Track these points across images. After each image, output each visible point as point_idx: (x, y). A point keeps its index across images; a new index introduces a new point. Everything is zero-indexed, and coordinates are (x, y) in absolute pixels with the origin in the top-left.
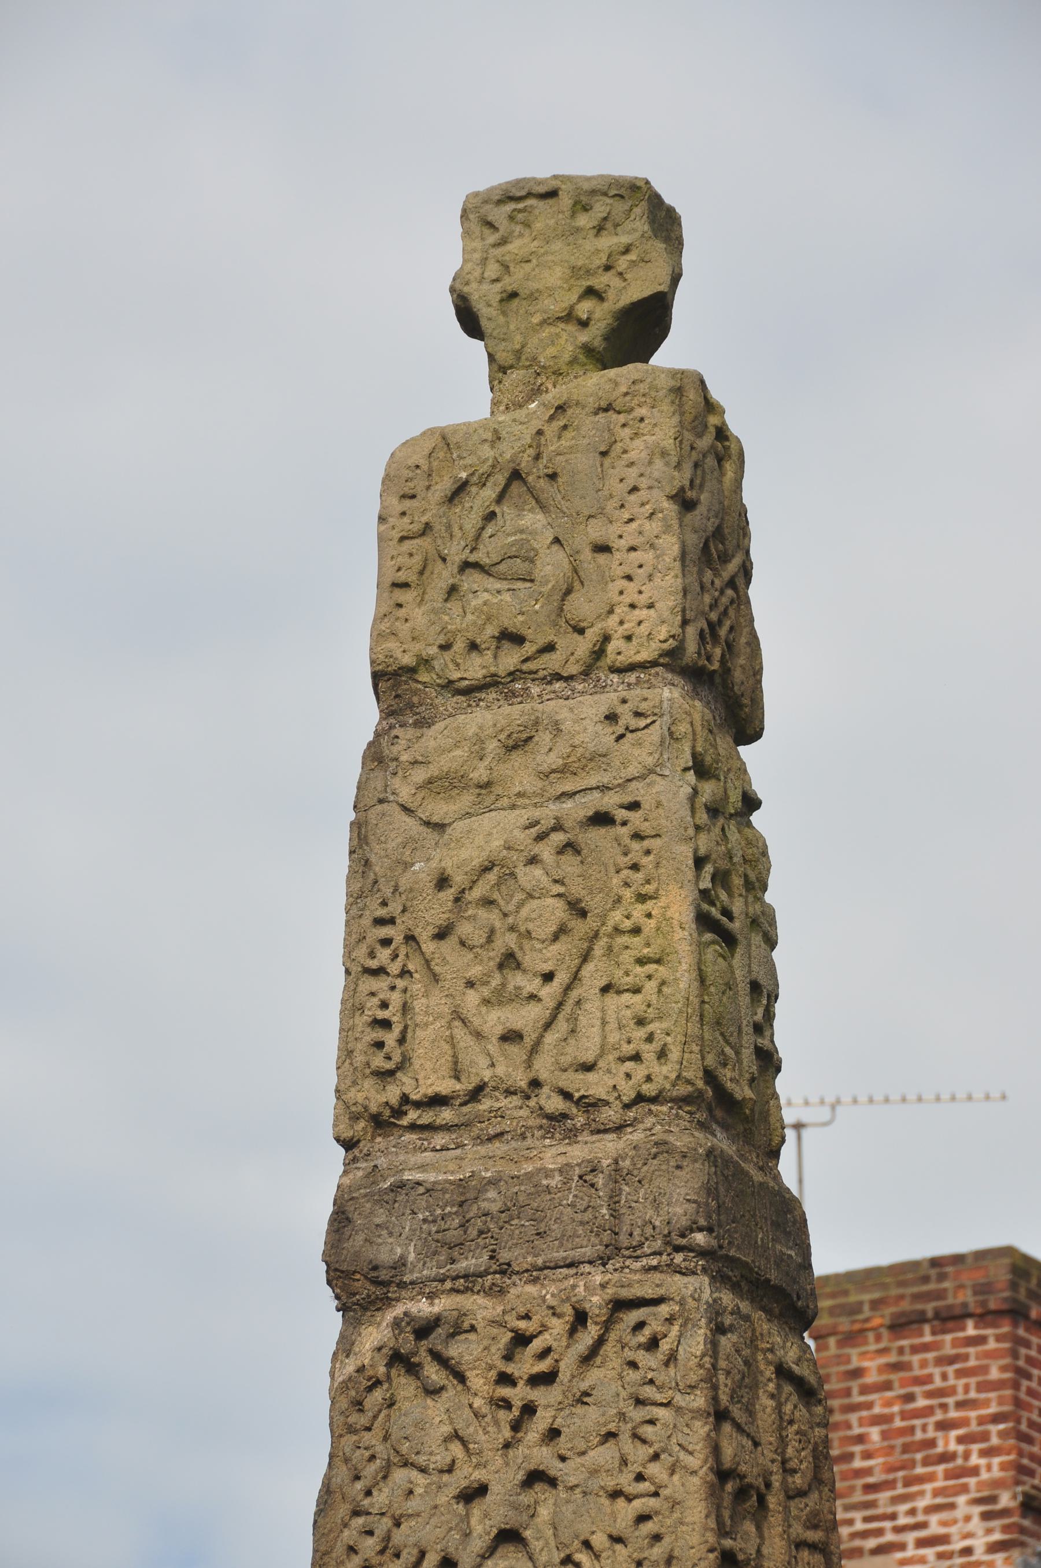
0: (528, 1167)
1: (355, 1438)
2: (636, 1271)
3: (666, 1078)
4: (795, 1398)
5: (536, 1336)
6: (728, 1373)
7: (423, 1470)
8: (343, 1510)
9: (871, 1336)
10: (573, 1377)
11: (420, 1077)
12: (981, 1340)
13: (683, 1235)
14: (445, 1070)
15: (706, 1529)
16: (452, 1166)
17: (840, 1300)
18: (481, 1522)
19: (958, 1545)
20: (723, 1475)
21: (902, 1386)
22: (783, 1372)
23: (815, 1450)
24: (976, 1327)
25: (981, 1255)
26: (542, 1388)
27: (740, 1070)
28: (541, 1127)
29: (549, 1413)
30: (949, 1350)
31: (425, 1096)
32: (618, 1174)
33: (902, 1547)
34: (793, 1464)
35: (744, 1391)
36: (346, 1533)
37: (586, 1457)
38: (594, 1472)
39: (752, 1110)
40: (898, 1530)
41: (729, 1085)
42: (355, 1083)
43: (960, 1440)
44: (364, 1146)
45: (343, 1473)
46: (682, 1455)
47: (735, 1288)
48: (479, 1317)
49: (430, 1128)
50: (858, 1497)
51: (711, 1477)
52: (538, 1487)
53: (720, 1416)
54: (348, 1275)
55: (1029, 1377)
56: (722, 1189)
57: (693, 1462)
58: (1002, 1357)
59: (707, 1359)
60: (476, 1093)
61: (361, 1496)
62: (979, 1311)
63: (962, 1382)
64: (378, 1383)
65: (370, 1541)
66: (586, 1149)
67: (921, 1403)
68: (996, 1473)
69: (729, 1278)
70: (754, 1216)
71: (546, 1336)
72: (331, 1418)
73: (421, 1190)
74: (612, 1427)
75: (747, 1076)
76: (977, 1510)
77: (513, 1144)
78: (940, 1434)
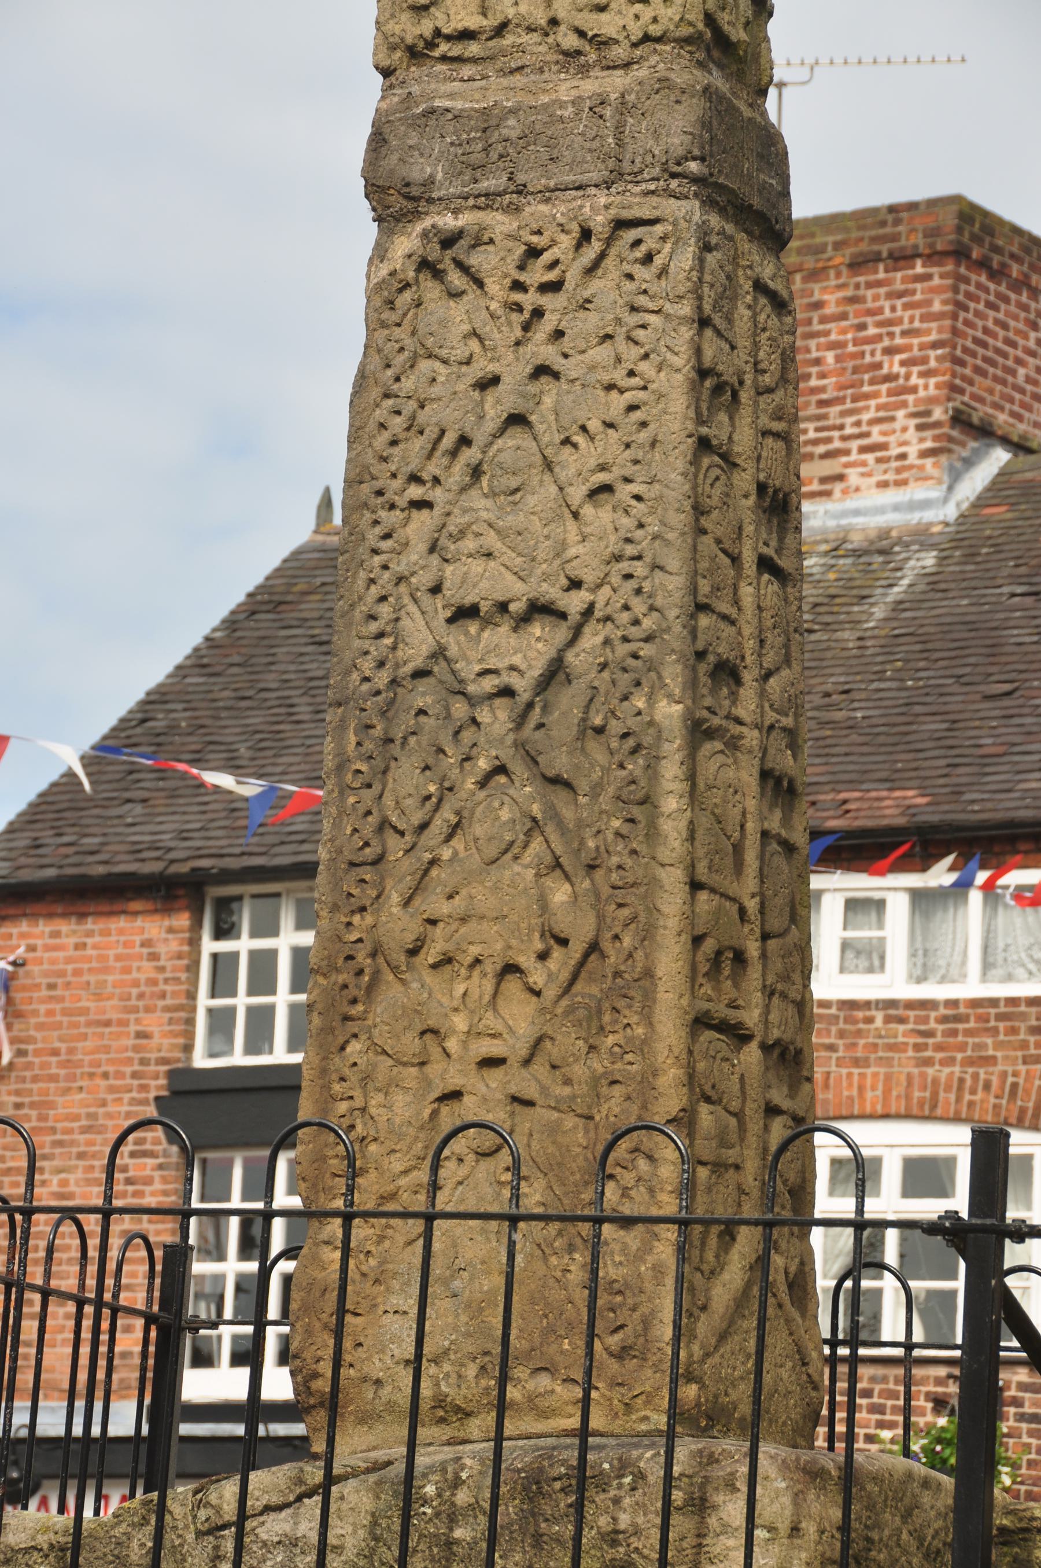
0: (545, 99)
1: (387, 332)
2: (636, 195)
3: (671, 19)
4: (768, 309)
5: (546, 250)
6: (712, 286)
7: (445, 362)
8: (375, 393)
9: (832, 273)
10: (577, 286)
11: (451, 12)
12: (928, 277)
13: (679, 164)
14: (474, 7)
15: (686, 418)
16: (477, 96)
17: (807, 241)
18: (493, 407)
19: (894, 451)
20: (703, 373)
21: (856, 316)
22: (759, 287)
23: (783, 354)
24: (924, 266)
25: (933, 203)
26: (550, 295)
27: (737, 14)
28: (557, 62)
29: (556, 317)
30: (899, 286)
31: (455, 30)
32: (624, 107)
33: (847, 452)
34: (763, 366)
35: (725, 302)
36: (378, 412)
37: (586, 355)
38: (592, 368)
39: (745, 51)
40: (844, 438)
41: (726, 28)
42: (393, 16)
43: (903, 363)
44: (400, 74)
45: (376, 361)
46: (669, 355)
47: (722, 211)
48: (497, 231)
49: (459, 60)
50: (813, 410)
51: (693, 375)
52: (544, 379)
53: (704, 322)
54: (383, 190)
55: (966, 309)
56: (715, 123)
57: (678, 361)
58: (945, 292)
59: (694, 273)
60: (501, 29)
61: (391, 382)
62: (927, 251)
63: (907, 314)
64: (408, 285)
65: (398, 420)
66: (597, 83)
67: (872, 331)
68: (932, 391)
69: (717, 203)
70: (742, 148)
71: (555, 249)
72: (367, 314)
73: (450, 116)
74: (609, 330)
75: (743, 20)
76: (913, 422)
77: (533, 77)
78: (886, 358)
